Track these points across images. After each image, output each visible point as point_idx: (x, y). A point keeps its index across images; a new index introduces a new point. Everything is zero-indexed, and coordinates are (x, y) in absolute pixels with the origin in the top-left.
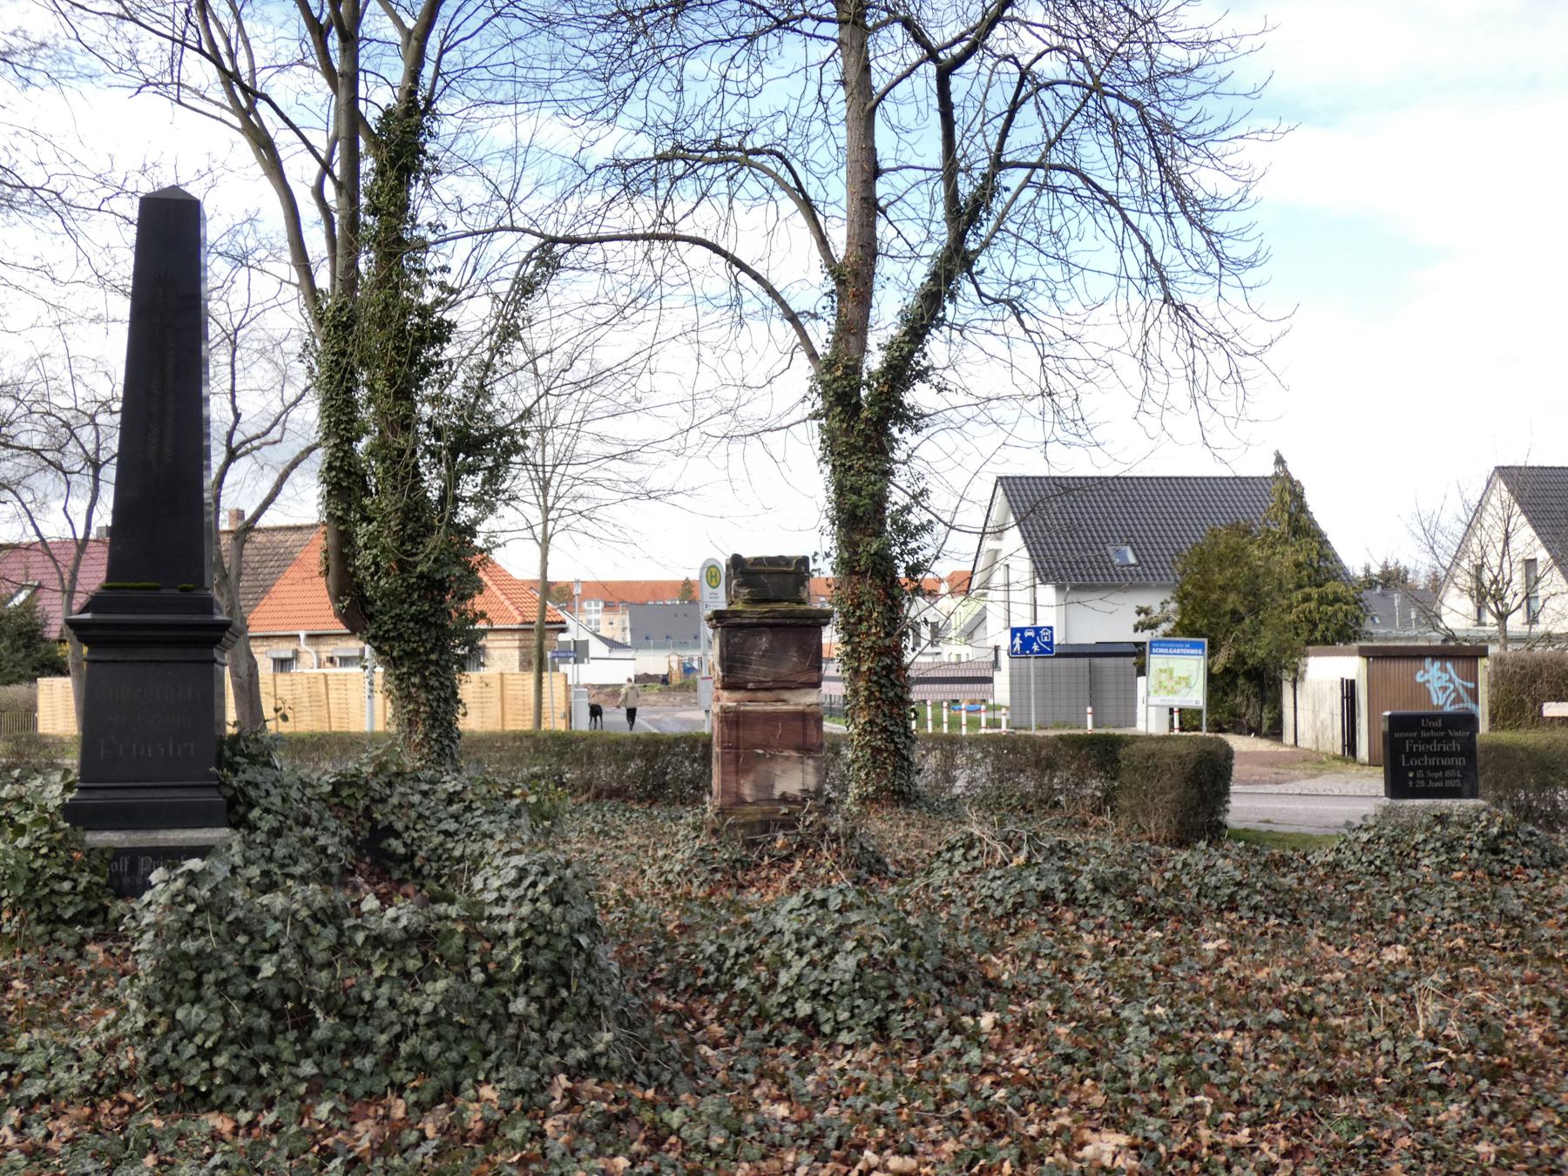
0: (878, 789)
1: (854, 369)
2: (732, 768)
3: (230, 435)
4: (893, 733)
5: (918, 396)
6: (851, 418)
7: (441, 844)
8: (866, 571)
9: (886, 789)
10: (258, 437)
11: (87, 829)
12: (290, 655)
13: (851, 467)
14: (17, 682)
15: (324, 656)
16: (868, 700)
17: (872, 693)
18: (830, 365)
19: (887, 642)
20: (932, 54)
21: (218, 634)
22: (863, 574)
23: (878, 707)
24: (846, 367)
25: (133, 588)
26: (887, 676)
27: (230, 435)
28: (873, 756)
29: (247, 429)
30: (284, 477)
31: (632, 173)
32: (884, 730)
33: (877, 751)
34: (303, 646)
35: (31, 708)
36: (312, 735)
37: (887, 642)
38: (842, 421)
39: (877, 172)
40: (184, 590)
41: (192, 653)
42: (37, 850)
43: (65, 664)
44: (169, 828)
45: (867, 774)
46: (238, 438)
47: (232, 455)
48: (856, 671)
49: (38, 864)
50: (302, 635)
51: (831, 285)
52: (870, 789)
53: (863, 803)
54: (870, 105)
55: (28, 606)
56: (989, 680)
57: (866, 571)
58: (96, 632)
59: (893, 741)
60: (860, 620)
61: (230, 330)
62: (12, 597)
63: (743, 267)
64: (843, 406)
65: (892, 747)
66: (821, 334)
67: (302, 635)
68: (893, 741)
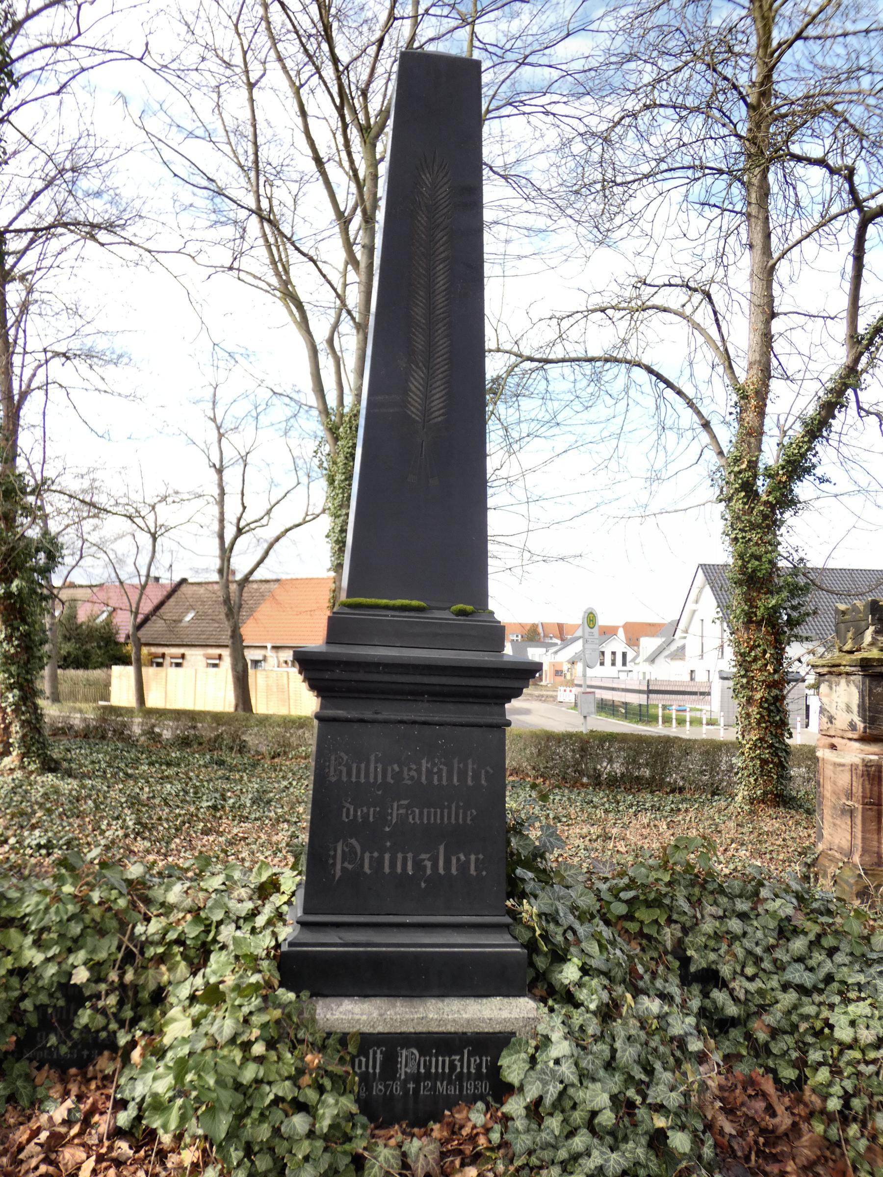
0: (765, 793)
1: (753, 465)
2: (873, 826)
3: (239, 520)
4: (777, 748)
5: (803, 489)
6: (752, 502)
7: (795, 1007)
8: (762, 620)
9: (772, 792)
10: (256, 521)
11: (317, 994)
12: (261, 658)
13: (750, 540)
14: (99, 667)
15: (282, 660)
16: (759, 723)
17: (762, 716)
18: (737, 460)
19: (776, 677)
20: (857, 203)
21: (516, 684)
22: (759, 623)
23: (766, 728)
24: (749, 462)
25: (387, 607)
26: (774, 704)
27: (239, 520)
28: (761, 766)
29: (248, 517)
30: (271, 546)
31: (565, 324)
32: (771, 746)
33: (764, 762)
34: (269, 653)
35: (107, 684)
36: (300, 718)
37: (776, 677)
38: (745, 504)
39: (773, 315)
40: (462, 613)
41: (472, 713)
42: (246, 1046)
43: (130, 657)
44: (442, 995)
45: (756, 780)
46: (242, 524)
47: (240, 532)
48: (750, 700)
49: (249, 1073)
50: (269, 646)
51: (735, 398)
52: (759, 792)
53: (752, 803)
54: (771, 262)
55: (108, 623)
56: (709, 694)
57: (762, 620)
58: (337, 674)
59: (777, 755)
60: (755, 660)
61: (243, 454)
62: (98, 616)
63: (669, 384)
64: (746, 492)
65: (776, 760)
66: (727, 435)
67: (269, 646)
68: (777, 755)
